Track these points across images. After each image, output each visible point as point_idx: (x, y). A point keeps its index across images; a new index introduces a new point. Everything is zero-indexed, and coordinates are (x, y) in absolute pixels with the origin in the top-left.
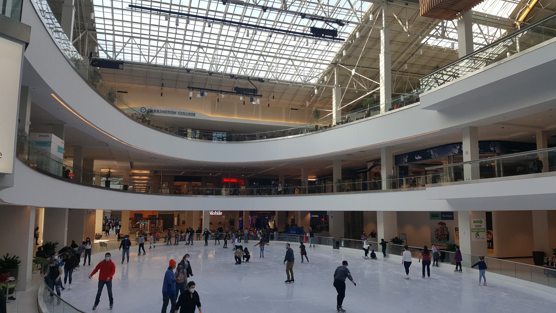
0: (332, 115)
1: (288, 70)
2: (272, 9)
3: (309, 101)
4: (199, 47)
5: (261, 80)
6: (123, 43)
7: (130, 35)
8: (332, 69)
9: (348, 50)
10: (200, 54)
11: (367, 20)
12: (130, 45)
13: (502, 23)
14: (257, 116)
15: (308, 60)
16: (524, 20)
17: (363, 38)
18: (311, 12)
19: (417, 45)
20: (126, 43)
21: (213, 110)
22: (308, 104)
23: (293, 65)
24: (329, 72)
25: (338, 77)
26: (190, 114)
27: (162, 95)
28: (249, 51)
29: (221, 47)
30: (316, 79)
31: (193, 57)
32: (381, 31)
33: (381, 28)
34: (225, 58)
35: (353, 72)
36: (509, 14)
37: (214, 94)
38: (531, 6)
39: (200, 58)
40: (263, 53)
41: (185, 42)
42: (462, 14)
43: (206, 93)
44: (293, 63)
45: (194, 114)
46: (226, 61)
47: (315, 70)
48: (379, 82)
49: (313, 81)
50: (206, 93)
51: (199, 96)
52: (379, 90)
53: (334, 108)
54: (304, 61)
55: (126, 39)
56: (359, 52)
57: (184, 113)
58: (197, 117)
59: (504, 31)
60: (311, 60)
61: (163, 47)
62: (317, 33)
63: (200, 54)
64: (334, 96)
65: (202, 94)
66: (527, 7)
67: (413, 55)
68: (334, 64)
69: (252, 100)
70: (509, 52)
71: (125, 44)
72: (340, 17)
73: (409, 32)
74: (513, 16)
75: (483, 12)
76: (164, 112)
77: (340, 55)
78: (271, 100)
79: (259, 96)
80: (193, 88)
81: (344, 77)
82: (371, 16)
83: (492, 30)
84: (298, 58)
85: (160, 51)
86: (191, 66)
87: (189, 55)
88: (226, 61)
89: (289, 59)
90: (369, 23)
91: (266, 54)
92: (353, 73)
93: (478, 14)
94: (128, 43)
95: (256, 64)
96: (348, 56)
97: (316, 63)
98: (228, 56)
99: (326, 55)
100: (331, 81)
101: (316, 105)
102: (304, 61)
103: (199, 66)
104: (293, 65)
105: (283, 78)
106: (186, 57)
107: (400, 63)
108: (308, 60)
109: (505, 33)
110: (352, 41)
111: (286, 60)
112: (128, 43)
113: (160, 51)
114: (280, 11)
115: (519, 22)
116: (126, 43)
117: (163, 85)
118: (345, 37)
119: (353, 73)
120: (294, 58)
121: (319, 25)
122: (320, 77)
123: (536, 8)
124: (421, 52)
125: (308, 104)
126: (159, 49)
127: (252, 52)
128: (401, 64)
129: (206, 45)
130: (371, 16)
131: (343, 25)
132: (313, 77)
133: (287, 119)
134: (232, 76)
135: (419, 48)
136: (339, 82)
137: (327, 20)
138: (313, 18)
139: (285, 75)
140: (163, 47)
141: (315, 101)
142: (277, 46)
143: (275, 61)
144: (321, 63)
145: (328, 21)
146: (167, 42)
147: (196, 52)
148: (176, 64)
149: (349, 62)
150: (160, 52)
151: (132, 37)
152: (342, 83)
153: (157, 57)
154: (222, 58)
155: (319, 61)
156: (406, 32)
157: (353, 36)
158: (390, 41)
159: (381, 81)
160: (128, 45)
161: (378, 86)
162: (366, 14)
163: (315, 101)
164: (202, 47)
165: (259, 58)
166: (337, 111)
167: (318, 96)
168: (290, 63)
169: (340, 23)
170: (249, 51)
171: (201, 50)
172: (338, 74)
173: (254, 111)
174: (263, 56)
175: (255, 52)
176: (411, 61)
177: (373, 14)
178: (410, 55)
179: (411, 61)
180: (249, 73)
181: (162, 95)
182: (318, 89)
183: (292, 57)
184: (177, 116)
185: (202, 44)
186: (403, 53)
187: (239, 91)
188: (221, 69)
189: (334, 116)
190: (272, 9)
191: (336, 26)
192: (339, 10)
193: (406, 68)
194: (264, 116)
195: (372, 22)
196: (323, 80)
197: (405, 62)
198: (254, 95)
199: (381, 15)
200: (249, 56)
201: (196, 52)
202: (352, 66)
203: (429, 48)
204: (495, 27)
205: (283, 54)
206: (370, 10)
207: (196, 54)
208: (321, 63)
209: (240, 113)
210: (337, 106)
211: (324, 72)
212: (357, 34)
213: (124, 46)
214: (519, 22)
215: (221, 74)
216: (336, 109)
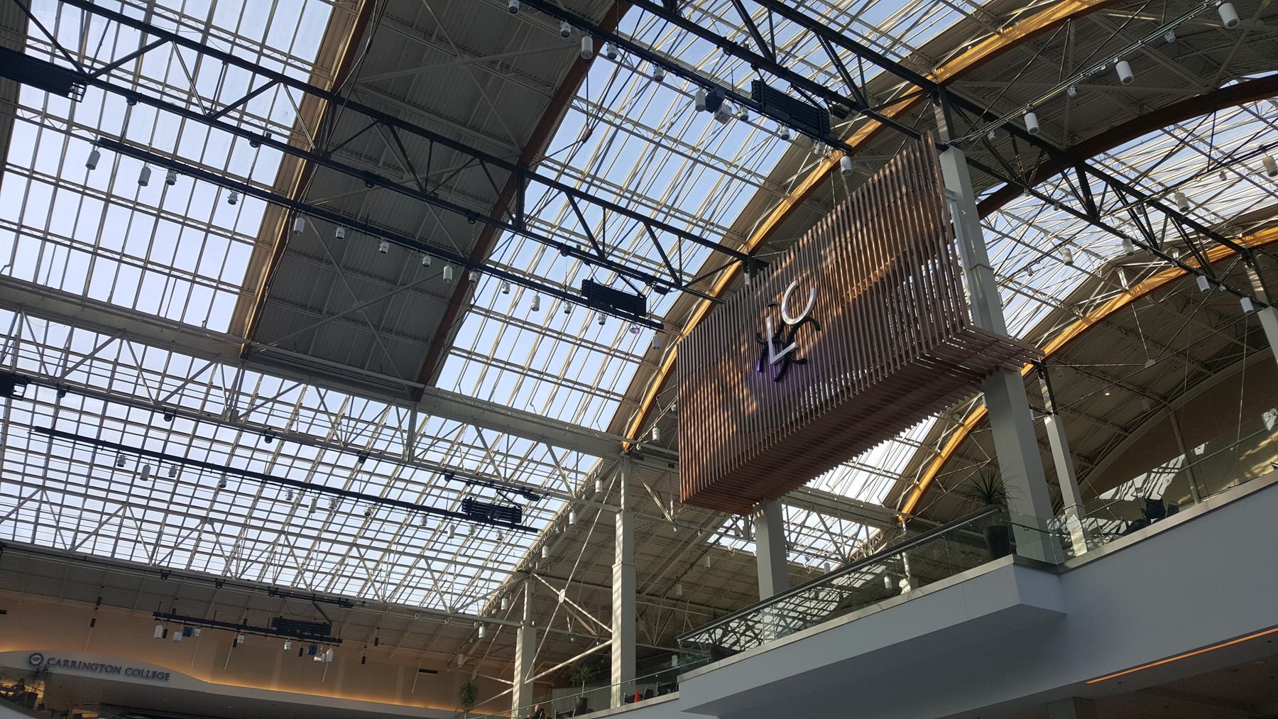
0: (511, 694)
1: (415, 579)
2: (381, 456)
3: (465, 654)
4: (205, 520)
5: (344, 602)
6: (20, 498)
7: (40, 482)
8: (520, 583)
9: (554, 548)
10: (204, 536)
11: (589, 489)
12: (36, 505)
13: (864, 513)
14: (330, 685)
15: (464, 560)
16: (914, 511)
17: (584, 523)
18: (470, 465)
19: (699, 545)
20: (26, 500)
21: (219, 668)
22: (461, 660)
23: (429, 569)
24: (511, 591)
25: (531, 603)
26: (155, 675)
27: (92, 625)
28: (325, 535)
29: (260, 524)
30: (481, 602)
31: (187, 541)
32: (618, 516)
33: (616, 509)
34: (264, 546)
35: (562, 595)
36: (883, 497)
37: (217, 632)
38: (922, 486)
39: (202, 544)
40: (360, 541)
41: (172, 507)
42: (762, 507)
43: (197, 631)
44: (429, 565)
45: (166, 676)
46: (266, 555)
47: (481, 583)
48: (610, 627)
49: (475, 610)
50: (197, 631)
51: (178, 635)
52: (610, 646)
53: (517, 679)
54: (456, 563)
55: (27, 492)
56: (570, 555)
57: (139, 673)
58: (172, 684)
59: (874, 531)
60: (472, 561)
61: (115, 515)
62: (476, 512)
63: (204, 536)
64: (519, 647)
65: (187, 633)
66: (916, 486)
67: (692, 565)
68: (524, 573)
69: (313, 652)
70: (889, 575)
71: (22, 500)
72: (536, 480)
73: (675, 522)
74: (891, 500)
75: (827, 489)
76: (88, 667)
77: (535, 555)
78: (371, 646)
79: (334, 640)
80: (171, 616)
81: (544, 602)
82: (598, 484)
83: (850, 527)
84: (441, 556)
85: (106, 522)
86: (179, 561)
87: (178, 536)
88: (266, 555)
89: (420, 556)
90: (593, 499)
91: (367, 543)
92: (561, 600)
93: (817, 493)
94: (30, 499)
95: (341, 563)
96: (554, 559)
97: (483, 568)
98: (275, 543)
99: (505, 552)
100: (518, 608)
101: (482, 662)
102: (456, 563)
103: (199, 564)
104: (429, 569)
105: (404, 596)
106: (168, 540)
107: (667, 579)
108: (464, 560)
109: (878, 535)
110: (561, 530)
111: (414, 559)
112: (30, 499)
113: (106, 522)
114: (401, 461)
115: (903, 515)
116: (26, 500)
117: (99, 602)
118: (543, 525)
119: (561, 600)
120: (433, 554)
121: (487, 495)
122: (491, 598)
123: (932, 489)
124: (708, 561)
125: (461, 660)
126: (105, 518)
127: (332, 537)
128: (670, 583)
129: (222, 517)
130: (598, 484)
131: (537, 499)
132: (475, 600)
133: (406, 696)
134: (274, 591)
135: (705, 552)
136: (532, 613)
137: (504, 486)
138: (474, 478)
139: (409, 590)
140: (115, 515)
141: (480, 654)
142: (394, 528)
143: (385, 559)
144: (493, 570)
145: (503, 489)
146: (126, 504)
147: (196, 530)
148: (141, 556)
149: (558, 569)
150: (105, 527)
151: (43, 488)
152: (540, 615)
153: (97, 535)
154: (259, 546)
155: (490, 565)
156: (669, 523)
157: (562, 520)
158: (637, 538)
159: (614, 626)
160: (28, 504)
161: (610, 636)
162: (589, 479)
163: (480, 654)
164: (212, 521)
165: (350, 550)
166: (523, 687)
167: (486, 641)
168: (422, 563)
169: (530, 493)
170: (325, 535)
171: (208, 527)
172: (531, 595)
173: (324, 676)
174: (358, 546)
175: (340, 538)
176: (692, 576)
177: (603, 479)
178: (687, 566)
179: (692, 576)
180: (320, 584)
181: (92, 625)
182: (486, 625)
183: (427, 553)
184: (120, 678)
185: (212, 515)
186: (671, 559)
187: (283, 627)
188: (252, 574)
189: (516, 697)
190: (381, 456)
191: (520, 499)
192: (532, 465)
193: (680, 592)
194: (348, 688)
195: (602, 494)
196: (498, 606)
197: (678, 580)
198: (321, 639)
199: (618, 483)
200: (325, 546)
201: (196, 530)
202: (559, 581)
203: (725, 553)
204: (856, 521)
205: (406, 545)
206: (596, 470)
207: (195, 535)
208: (493, 570)
209: (286, 679)
210: (523, 673)
211: (500, 589)
212: (571, 515)
213: (20, 505)
214: (903, 515)
215: (249, 585)
216: (522, 681)
